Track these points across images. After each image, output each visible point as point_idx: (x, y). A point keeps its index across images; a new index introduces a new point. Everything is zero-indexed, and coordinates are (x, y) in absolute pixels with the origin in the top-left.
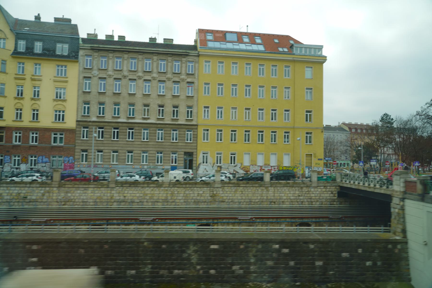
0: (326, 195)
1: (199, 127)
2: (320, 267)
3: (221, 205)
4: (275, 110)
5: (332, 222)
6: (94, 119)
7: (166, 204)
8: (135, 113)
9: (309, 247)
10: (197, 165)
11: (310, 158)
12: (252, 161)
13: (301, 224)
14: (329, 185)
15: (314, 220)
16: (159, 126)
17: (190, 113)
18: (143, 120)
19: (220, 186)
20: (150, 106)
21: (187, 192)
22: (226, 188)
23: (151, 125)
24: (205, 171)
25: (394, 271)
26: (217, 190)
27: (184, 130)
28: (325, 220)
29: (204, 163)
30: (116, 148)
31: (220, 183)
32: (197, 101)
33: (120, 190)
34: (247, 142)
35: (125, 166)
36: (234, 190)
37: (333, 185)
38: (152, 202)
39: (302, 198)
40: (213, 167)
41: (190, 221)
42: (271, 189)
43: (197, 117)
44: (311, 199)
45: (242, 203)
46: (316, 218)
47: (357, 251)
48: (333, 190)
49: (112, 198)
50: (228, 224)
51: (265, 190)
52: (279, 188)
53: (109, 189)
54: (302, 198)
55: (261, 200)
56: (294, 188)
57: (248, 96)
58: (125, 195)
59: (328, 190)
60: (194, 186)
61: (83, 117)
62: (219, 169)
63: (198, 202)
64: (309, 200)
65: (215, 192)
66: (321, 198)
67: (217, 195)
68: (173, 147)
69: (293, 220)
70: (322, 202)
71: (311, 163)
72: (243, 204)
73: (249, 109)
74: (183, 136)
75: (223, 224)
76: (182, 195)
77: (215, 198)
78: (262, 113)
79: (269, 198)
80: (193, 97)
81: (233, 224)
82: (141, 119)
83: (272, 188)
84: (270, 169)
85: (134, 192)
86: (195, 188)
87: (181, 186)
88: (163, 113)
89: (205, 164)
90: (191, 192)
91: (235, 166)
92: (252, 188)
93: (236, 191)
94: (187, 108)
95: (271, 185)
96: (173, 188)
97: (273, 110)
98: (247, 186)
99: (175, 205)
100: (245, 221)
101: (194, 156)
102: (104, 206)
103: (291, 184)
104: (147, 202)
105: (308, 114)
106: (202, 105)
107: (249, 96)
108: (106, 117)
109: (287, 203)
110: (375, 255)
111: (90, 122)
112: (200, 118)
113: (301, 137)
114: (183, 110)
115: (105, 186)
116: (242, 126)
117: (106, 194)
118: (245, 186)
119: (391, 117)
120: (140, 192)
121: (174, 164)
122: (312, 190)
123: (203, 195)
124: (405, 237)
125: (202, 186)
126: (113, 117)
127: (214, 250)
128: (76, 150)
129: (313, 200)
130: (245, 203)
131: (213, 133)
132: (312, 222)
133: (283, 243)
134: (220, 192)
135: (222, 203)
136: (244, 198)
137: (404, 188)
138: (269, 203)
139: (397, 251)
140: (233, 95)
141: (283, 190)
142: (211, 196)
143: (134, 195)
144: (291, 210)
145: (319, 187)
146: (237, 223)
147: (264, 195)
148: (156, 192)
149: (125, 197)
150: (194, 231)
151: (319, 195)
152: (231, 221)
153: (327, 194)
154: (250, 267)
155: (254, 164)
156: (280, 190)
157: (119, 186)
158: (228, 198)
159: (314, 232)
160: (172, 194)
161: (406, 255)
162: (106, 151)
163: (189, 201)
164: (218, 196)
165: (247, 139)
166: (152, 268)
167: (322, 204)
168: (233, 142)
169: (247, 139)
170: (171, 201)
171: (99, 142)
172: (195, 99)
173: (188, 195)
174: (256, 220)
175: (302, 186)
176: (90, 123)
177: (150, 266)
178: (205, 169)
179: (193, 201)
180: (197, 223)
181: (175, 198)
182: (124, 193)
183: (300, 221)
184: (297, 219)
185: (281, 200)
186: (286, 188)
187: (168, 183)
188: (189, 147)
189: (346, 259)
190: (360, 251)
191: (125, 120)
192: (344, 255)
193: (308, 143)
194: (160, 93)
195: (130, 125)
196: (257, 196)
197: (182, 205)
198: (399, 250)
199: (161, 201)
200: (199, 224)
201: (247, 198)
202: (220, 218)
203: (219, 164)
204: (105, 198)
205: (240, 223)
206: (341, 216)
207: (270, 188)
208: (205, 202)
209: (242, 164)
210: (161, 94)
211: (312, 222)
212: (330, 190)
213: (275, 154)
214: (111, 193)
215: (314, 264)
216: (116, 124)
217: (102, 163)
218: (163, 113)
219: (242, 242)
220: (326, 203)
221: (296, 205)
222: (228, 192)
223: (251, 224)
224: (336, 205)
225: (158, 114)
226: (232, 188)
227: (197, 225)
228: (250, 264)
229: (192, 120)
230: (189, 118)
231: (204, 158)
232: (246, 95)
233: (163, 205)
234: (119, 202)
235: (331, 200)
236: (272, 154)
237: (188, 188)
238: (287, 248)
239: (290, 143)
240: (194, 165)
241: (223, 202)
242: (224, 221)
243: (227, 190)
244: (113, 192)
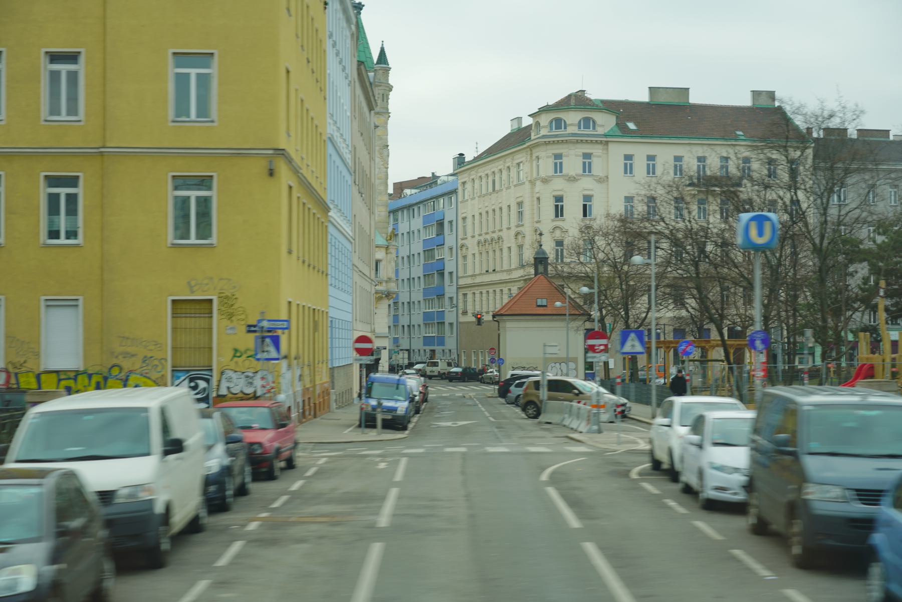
11: (202, 322)
236: (51, 304)
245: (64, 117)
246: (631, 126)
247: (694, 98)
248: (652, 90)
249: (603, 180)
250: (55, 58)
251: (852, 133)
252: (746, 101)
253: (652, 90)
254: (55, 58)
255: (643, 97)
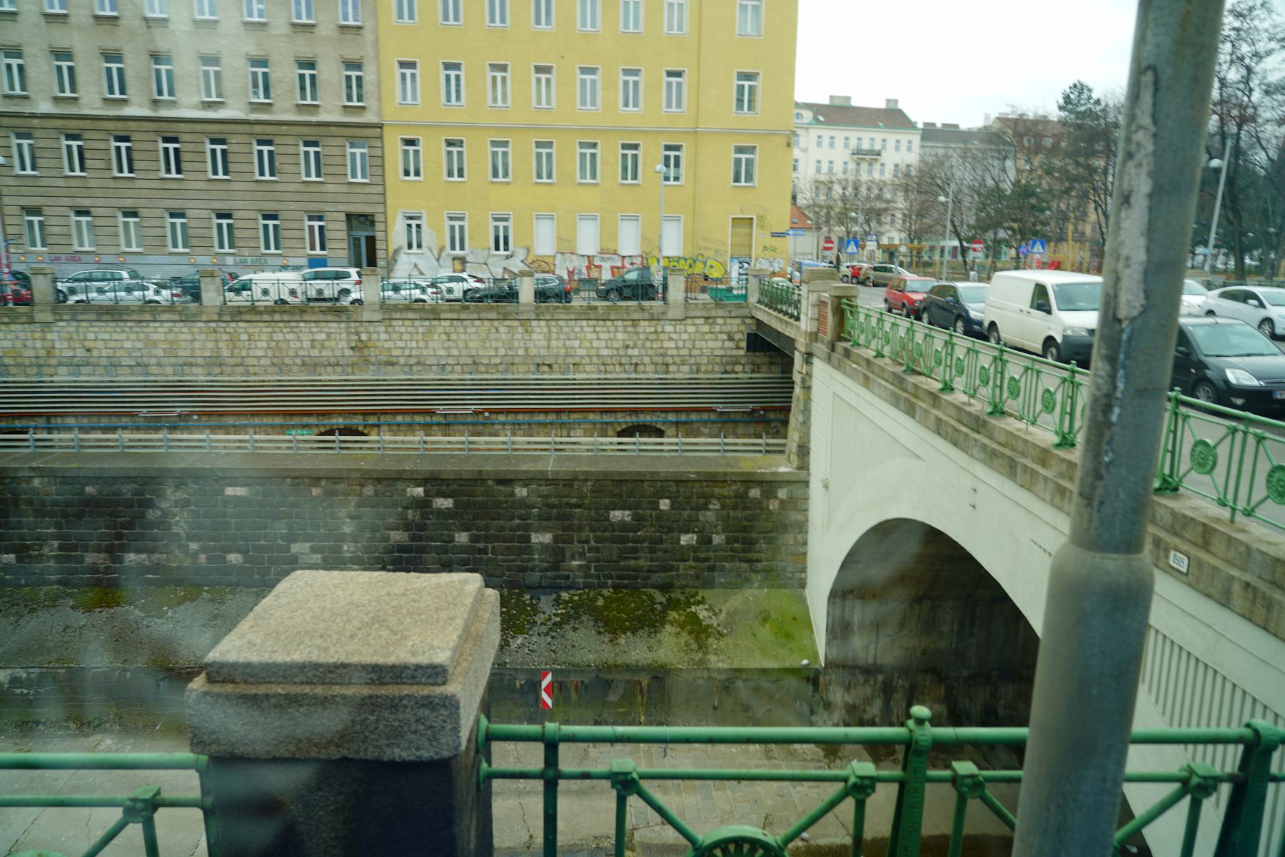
0: (711, 344)
1: (385, 129)
2: (544, 547)
3: (385, 374)
4: (636, 72)
5: (726, 423)
6: (46, 107)
7: (217, 370)
8: (177, 87)
9: (513, 494)
10: (391, 254)
11: (746, 231)
12: (559, 238)
13: (628, 432)
14: (721, 312)
15: (672, 417)
16: (258, 129)
17: (355, 87)
18: (204, 109)
19: (377, 316)
20: (270, 64)
21: (279, 337)
22: (400, 323)
23: (233, 127)
24: (415, 273)
25: (759, 561)
26: (371, 329)
27: (340, 141)
28: (705, 416)
29: (410, 246)
30: (129, 203)
31: (377, 308)
32: (376, 42)
33: (72, 329)
34: (545, 180)
35: (165, 259)
36: (421, 330)
37: (733, 314)
38: (173, 365)
39: (636, 352)
40: (438, 260)
41: (296, 420)
42: (539, 327)
43: (379, 99)
44: (663, 355)
45: (449, 368)
46: (677, 411)
47: (656, 507)
48: (735, 329)
49: (49, 352)
50: (411, 427)
51: (520, 329)
52: (562, 323)
53: (37, 327)
54: (636, 352)
55: (508, 360)
56: (609, 323)
57: (543, 25)
58: (88, 344)
59: (718, 328)
60: (298, 318)
61: (8, 101)
62: (861, 277)
63: (315, 365)
64: (659, 360)
65: (364, 337)
66: (695, 352)
67: (369, 344)
68: (307, 197)
69: (607, 418)
70: (698, 365)
71: (750, 246)
72: (452, 372)
73: (547, 70)
74: (339, 160)
75: (396, 428)
76: (264, 344)
77: (366, 352)
78: (593, 82)
79: (533, 352)
80: (359, 28)
81: (427, 427)
82: (195, 107)
83: (543, 323)
84: (619, 264)
85: (115, 336)
86: (302, 324)
87: (258, 318)
88: (360, 86)
89: (415, 250)
90: (291, 336)
91: (508, 257)
92: (477, 323)
93: (429, 332)
94: (343, 67)
95: (538, 315)
96: (233, 324)
97: (627, 72)
98: (463, 316)
99: (248, 374)
100: (461, 419)
101: (379, 226)
102: (30, 376)
103: (600, 311)
104: (159, 365)
105: (746, 84)
106: (391, 59)
107: (548, 23)
108: (84, 101)
109: (588, 368)
110: (709, 516)
111: (33, 116)
112: (391, 102)
113: (719, 162)
114: (330, 73)
115: (23, 319)
116: (528, 129)
117: (29, 343)
118: (455, 316)
119: (1095, 96)
120: (133, 336)
121: (318, 252)
122: (669, 328)
123: (327, 344)
124: (804, 466)
125: (321, 317)
126: (106, 100)
127: (237, 500)
128: (7, 210)
129: (670, 360)
130: (458, 368)
131: (432, 152)
132: (664, 423)
133: (435, 483)
134: (380, 335)
135: (390, 368)
136: (455, 352)
137: (815, 324)
138: (533, 368)
139: (773, 505)
140: (492, 20)
141: (577, 329)
142: (352, 348)
143: (118, 345)
144: (602, 387)
145: (689, 321)
146: (438, 424)
147: (516, 344)
148: (182, 337)
149: (88, 350)
150: (312, 448)
151: (689, 345)
152: (419, 419)
153: (716, 340)
154: (341, 547)
155: (566, 246)
156: (566, 330)
157: (65, 317)
158: (407, 352)
159: (670, 453)
160: (233, 341)
161: (800, 518)
162: (101, 211)
163: (287, 361)
164: (375, 347)
165: (544, 169)
166: (61, 548)
167: (698, 371)
168: (501, 179)
169: (544, 169)
170: (232, 361)
171: (73, 183)
172: (368, 34)
173: (283, 345)
174: (494, 416)
175: (635, 316)
176: (36, 122)
177: (56, 543)
178: (416, 266)
179: (299, 361)
180: (317, 426)
181: (244, 353)
182: (85, 339)
183: (628, 419)
184: (619, 415)
185: (569, 360)
186: (584, 323)
187: (217, 310)
188: (361, 198)
189: (623, 526)
190: (665, 504)
191: (146, 112)
192: (616, 515)
193: (743, 183)
194: (250, 15)
195: (164, 126)
196: (496, 349)
197: (266, 373)
198: (782, 502)
199: (200, 361)
200: (323, 430)
201: (464, 352)
202: (385, 413)
203: (458, 252)
204: (31, 353)
205: (447, 426)
206: (751, 406)
207: (534, 323)
208: (338, 365)
209: (528, 250)
210: (256, 19)
211: (664, 423)
212: (725, 329)
213: (636, 218)
214: (44, 339)
215: (528, 539)
216: (119, 125)
217: (92, 249)
218: (360, 86)
219: (318, 479)
220: (710, 367)
221: (617, 374)
222: (406, 337)
223: (480, 428)
224: (743, 374)
225: (251, 89)
226: (417, 323)
227: (316, 431)
228: (342, 538)
229: (363, 108)
230: (355, 103)
231: (409, 232)
232: (538, 22)
233: (209, 374)
234: (75, 365)
235: (725, 359)
236: (624, 218)
237: (281, 325)
238: (446, 496)
239: (682, 181)
240: (380, 254)
241: (392, 364)
242: (399, 419)
243: (403, 329)
244: (49, 336)
245: (674, 109)
246: (821, 118)
247: (854, 103)
248: (831, 97)
249: (805, 150)
250: (670, 74)
251: (939, 125)
252: (883, 105)
253: (831, 97)
254: (670, 74)
255: (826, 102)
